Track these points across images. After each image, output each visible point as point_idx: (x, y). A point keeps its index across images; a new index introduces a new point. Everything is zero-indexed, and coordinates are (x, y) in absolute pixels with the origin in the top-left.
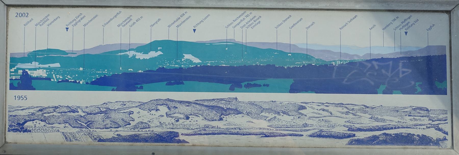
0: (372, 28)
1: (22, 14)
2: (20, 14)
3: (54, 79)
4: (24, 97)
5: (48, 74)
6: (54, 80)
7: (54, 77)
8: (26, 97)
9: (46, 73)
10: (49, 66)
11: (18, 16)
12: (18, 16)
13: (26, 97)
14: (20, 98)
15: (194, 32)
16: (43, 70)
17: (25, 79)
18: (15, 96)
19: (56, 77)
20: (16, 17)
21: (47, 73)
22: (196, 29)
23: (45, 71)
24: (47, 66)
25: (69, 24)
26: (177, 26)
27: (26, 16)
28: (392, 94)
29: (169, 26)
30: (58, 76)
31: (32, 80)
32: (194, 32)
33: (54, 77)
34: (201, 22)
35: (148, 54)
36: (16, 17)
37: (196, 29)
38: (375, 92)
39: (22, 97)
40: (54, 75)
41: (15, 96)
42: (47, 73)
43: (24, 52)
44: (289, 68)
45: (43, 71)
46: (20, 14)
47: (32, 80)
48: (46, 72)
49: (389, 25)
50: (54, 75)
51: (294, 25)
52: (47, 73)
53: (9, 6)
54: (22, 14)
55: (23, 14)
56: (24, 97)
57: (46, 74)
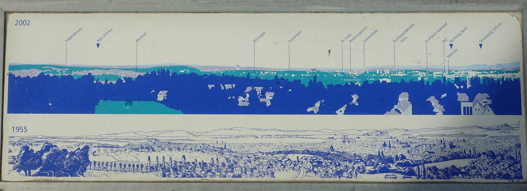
0: (292, 40)
1: (23, 24)
2: (21, 21)
4: (23, 128)
11: (18, 24)
12: (18, 24)
13: (25, 128)
14: (19, 129)
17: (343, 99)
18: (13, 127)
20: (16, 25)
22: (452, 44)
25: (454, 40)
28: (93, 112)
29: (343, 41)
31: (458, 100)
32: (98, 47)
35: (518, 73)
36: (16, 25)
37: (452, 44)
38: (303, 111)
39: (21, 128)
41: (13, 127)
44: (384, 82)
46: (25, 24)
47: (458, 100)
54: (23, 24)
55: (20, 21)
56: (23, 128)
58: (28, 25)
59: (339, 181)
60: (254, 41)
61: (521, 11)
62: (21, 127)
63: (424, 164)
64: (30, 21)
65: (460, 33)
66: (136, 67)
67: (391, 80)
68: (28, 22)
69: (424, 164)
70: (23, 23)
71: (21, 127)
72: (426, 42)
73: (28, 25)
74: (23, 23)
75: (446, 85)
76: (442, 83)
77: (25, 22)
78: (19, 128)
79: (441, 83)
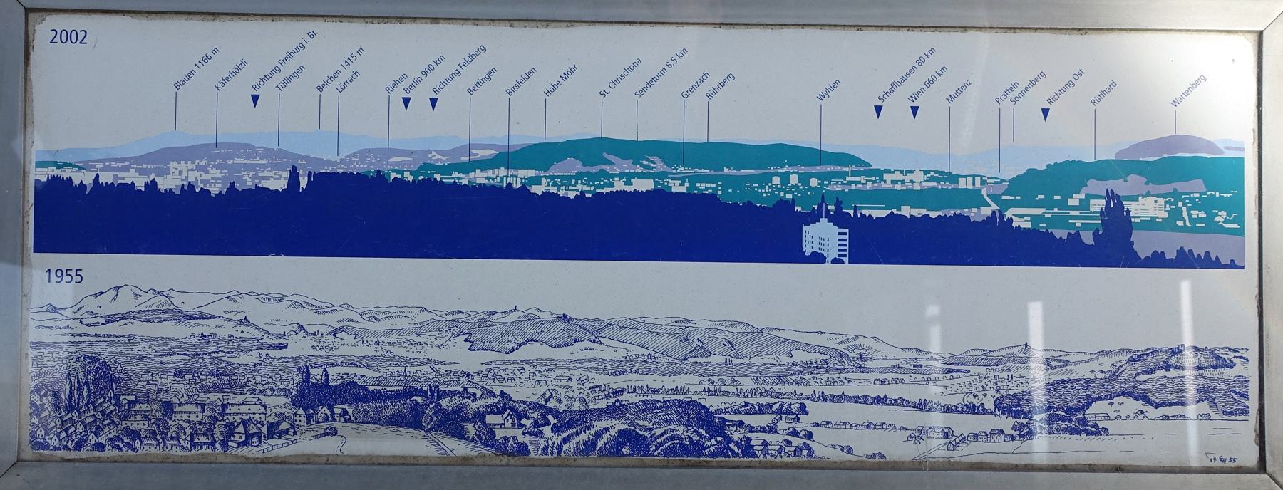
3: (1184, 220)
4: (73, 273)
5: (1169, 209)
6: (1185, 223)
7: (1185, 214)
8: (79, 273)
9: (1165, 207)
10: (1175, 189)
13: (79, 273)
15: (1045, 120)
16: (1155, 198)
18: (49, 270)
19: (1190, 215)
20: (51, 42)
21: (1168, 206)
23: (1161, 201)
24: (1167, 188)
26: (949, 98)
27: (80, 39)
30: (1197, 212)
32: (1045, 120)
33: (1185, 214)
34: (1069, 85)
35: (129, 172)
36: (51, 42)
40: (1184, 209)
41: (49, 270)
42: (1168, 209)
43: (507, 150)
45: (1156, 202)
48: (1166, 203)
49: (476, 54)
50: (1184, 209)
51: (894, 85)
52: (1168, 206)
53: (28, 11)
56: (73, 273)
57: (1165, 211)
58: (81, 43)
59: (1223, 468)
60: (319, 89)
61: (26, 9)
62: (67, 270)
63: (799, 416)
64: (86, 32)
65: (459, 68)
66: (507, 150)
67: (982, 206)
68: (81, 35)
69: (799, 416)
70: (69, 37)
71: (67, 270)
72: (217, 88)
73: (81, 43)
74: (69, 37)
75: (87, 193)
76: (87, 193)
77: (64, 39)
78: (62, 271)
79: (939, 216)
